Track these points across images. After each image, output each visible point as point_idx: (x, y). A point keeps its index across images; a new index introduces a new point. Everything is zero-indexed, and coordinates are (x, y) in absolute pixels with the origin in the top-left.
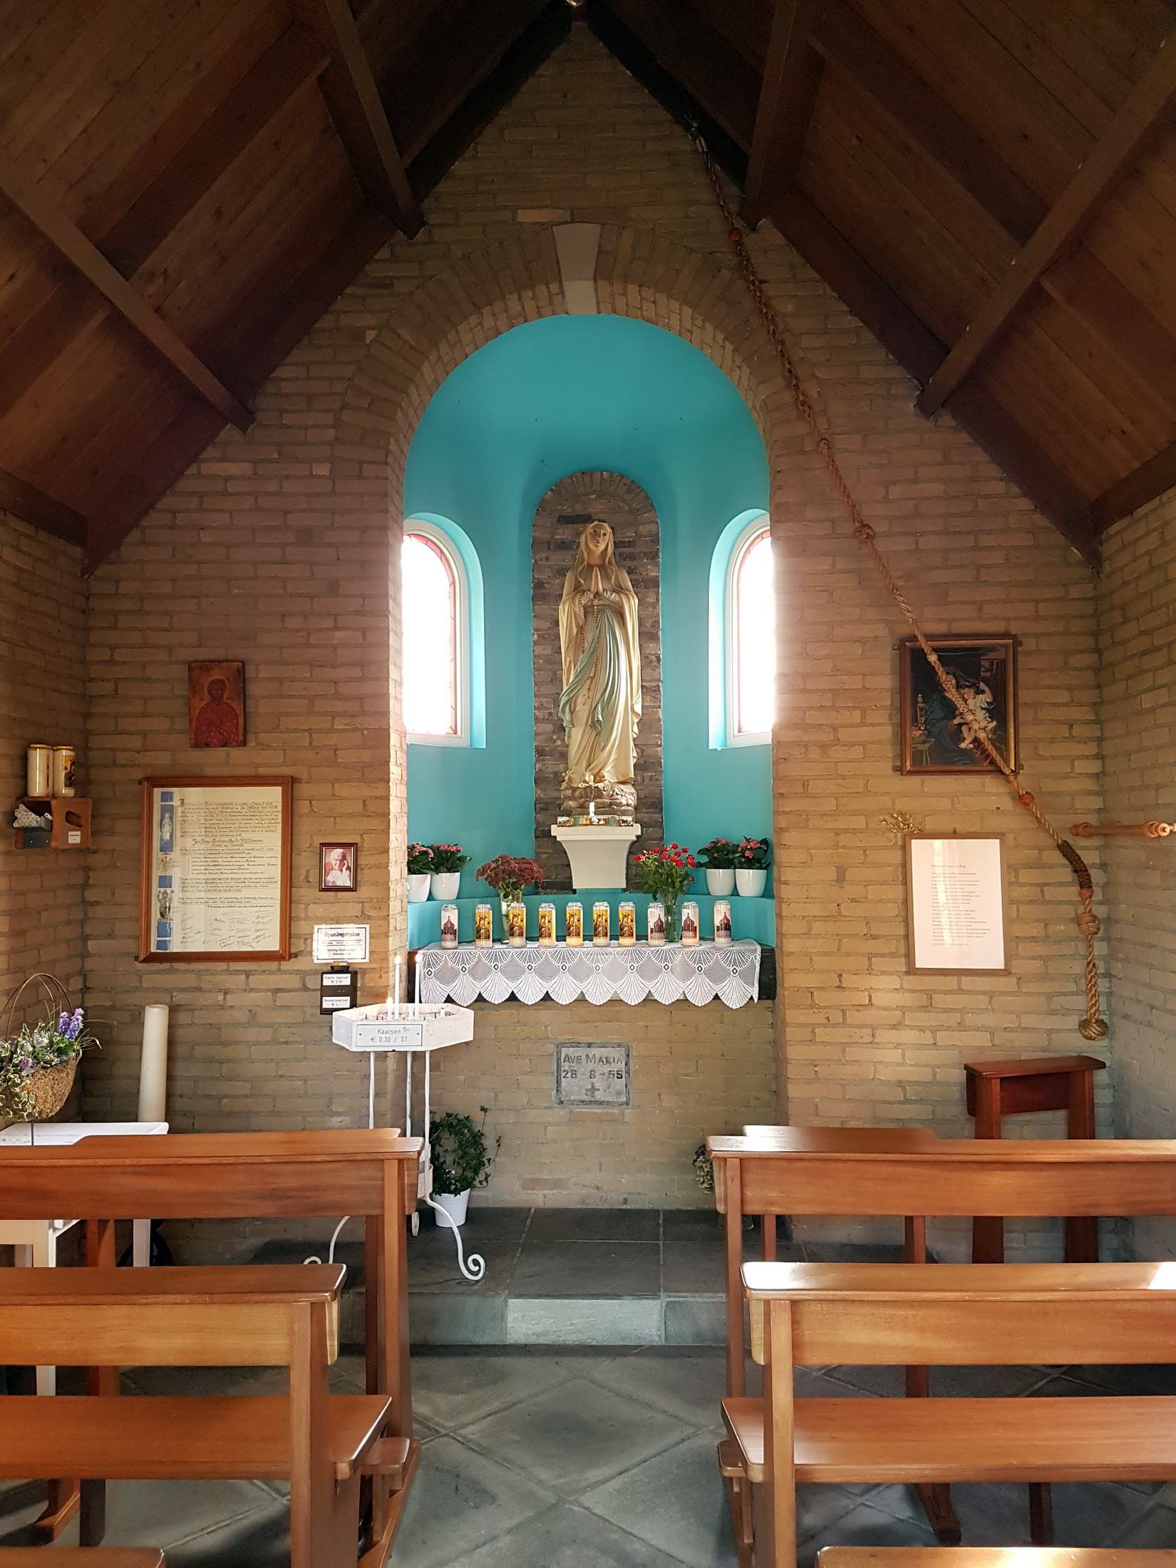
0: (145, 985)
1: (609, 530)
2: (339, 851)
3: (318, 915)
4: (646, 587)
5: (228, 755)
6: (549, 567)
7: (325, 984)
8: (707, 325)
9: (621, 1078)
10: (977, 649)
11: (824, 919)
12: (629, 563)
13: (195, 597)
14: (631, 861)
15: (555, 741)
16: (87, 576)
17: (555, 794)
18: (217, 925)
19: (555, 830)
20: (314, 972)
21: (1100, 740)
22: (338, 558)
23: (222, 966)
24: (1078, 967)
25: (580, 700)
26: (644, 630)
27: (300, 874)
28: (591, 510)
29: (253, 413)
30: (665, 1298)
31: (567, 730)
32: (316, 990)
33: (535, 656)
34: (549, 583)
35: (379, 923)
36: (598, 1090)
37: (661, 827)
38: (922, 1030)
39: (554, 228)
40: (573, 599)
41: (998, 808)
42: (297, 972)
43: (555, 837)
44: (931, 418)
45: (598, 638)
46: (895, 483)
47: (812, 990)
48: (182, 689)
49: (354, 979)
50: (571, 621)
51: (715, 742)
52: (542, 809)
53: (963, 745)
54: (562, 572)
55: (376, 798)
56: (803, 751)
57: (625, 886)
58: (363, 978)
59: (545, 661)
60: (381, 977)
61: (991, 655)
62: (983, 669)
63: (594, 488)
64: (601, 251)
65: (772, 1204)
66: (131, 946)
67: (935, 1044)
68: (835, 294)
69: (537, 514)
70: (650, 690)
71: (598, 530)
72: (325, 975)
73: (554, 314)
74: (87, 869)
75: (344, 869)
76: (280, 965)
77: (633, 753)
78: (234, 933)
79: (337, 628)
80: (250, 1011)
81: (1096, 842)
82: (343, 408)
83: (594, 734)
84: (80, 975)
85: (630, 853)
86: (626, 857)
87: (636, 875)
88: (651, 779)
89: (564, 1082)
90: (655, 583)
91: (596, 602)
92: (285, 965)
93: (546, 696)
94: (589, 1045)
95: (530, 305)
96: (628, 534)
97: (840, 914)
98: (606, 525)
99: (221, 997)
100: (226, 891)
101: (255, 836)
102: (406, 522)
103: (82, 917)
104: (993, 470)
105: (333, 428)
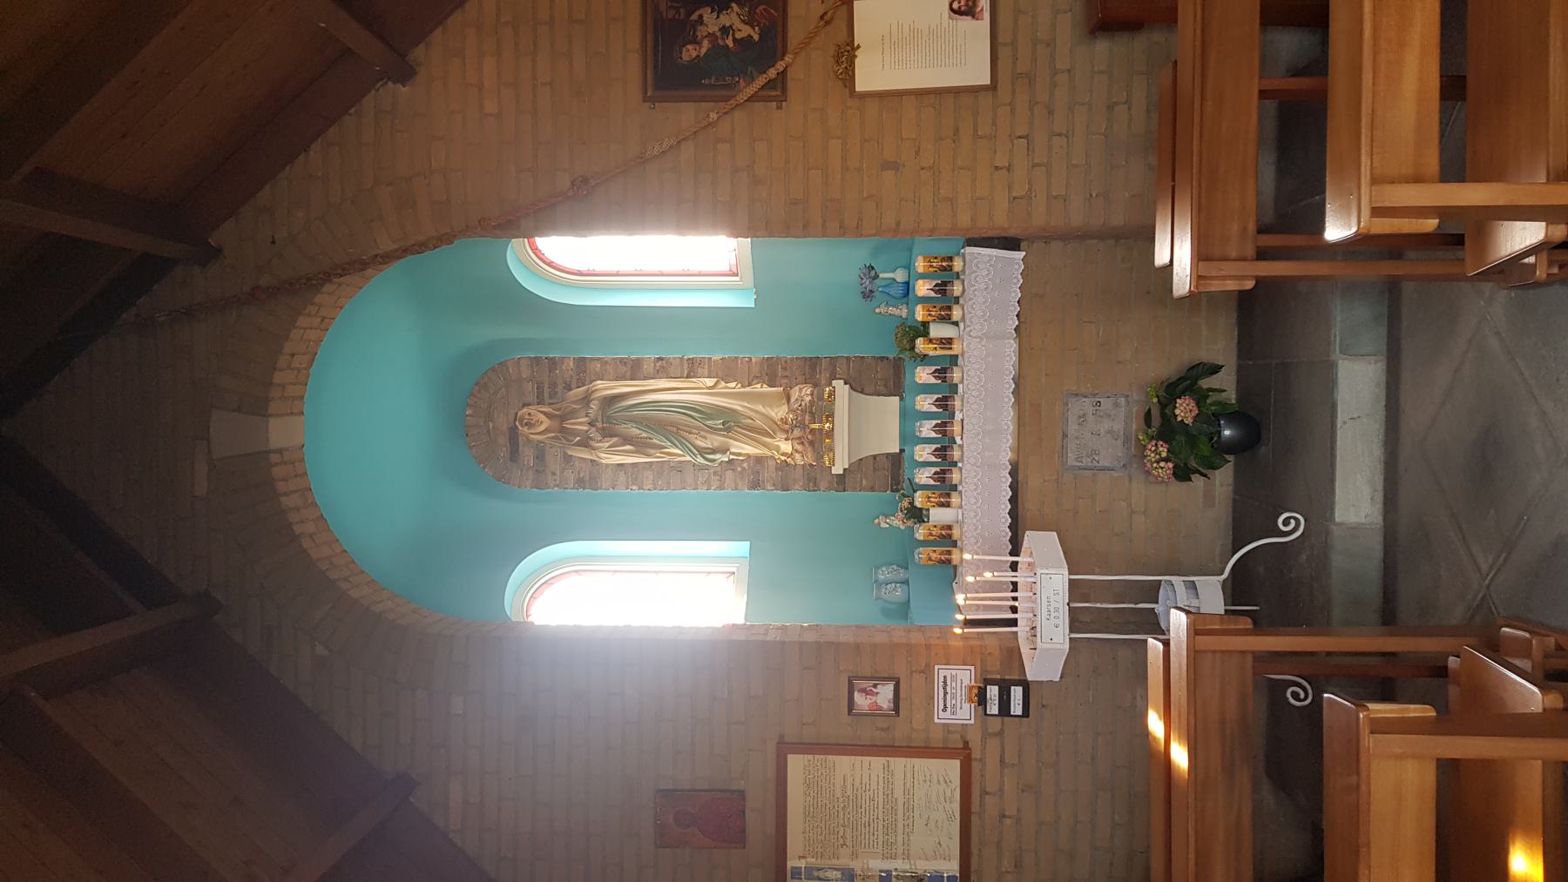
1: (525, 410)
4: (585, 372)
6: (562, 471)
7: (997, 713)
9: (1099, 402)
12: (560, 389)
14: (871, 392)
15: (744, 469)
17: (799, 471)
18: (932, 825)
19: (838, 470)
23: (975, 819)
26: (628, 374)
30: (1336, 355)
31: (731, 457)
32: (1003, 723)
33: (655, 489)
36: (1112, 427)
43: (845, 470)
45: (636, 423)
47: (1012, 198)
51: (747, 301)
52: (815, 484)
53: (756, 37)
54: (568, 459)
57: (898, 398)
60: (990, 654)
64: (239, 410)
65: (1245, 229)
67: (1069, 71)
68: (288, 168)
70: (691, 369)
71: (525, 421)
72: (988, 713)
73: (302, 460)
77: (758, 388)
80: (1023, 791)
83: (735, 428)
85: (862, 392)
88: (784, 369)
89: (1104, 463)
90: (581, 361)
91: (599, 425)
92: (976, 754)
94: (1065, 436)
98: (520, 413)
99: (1008, 821)
101: (839, 783)
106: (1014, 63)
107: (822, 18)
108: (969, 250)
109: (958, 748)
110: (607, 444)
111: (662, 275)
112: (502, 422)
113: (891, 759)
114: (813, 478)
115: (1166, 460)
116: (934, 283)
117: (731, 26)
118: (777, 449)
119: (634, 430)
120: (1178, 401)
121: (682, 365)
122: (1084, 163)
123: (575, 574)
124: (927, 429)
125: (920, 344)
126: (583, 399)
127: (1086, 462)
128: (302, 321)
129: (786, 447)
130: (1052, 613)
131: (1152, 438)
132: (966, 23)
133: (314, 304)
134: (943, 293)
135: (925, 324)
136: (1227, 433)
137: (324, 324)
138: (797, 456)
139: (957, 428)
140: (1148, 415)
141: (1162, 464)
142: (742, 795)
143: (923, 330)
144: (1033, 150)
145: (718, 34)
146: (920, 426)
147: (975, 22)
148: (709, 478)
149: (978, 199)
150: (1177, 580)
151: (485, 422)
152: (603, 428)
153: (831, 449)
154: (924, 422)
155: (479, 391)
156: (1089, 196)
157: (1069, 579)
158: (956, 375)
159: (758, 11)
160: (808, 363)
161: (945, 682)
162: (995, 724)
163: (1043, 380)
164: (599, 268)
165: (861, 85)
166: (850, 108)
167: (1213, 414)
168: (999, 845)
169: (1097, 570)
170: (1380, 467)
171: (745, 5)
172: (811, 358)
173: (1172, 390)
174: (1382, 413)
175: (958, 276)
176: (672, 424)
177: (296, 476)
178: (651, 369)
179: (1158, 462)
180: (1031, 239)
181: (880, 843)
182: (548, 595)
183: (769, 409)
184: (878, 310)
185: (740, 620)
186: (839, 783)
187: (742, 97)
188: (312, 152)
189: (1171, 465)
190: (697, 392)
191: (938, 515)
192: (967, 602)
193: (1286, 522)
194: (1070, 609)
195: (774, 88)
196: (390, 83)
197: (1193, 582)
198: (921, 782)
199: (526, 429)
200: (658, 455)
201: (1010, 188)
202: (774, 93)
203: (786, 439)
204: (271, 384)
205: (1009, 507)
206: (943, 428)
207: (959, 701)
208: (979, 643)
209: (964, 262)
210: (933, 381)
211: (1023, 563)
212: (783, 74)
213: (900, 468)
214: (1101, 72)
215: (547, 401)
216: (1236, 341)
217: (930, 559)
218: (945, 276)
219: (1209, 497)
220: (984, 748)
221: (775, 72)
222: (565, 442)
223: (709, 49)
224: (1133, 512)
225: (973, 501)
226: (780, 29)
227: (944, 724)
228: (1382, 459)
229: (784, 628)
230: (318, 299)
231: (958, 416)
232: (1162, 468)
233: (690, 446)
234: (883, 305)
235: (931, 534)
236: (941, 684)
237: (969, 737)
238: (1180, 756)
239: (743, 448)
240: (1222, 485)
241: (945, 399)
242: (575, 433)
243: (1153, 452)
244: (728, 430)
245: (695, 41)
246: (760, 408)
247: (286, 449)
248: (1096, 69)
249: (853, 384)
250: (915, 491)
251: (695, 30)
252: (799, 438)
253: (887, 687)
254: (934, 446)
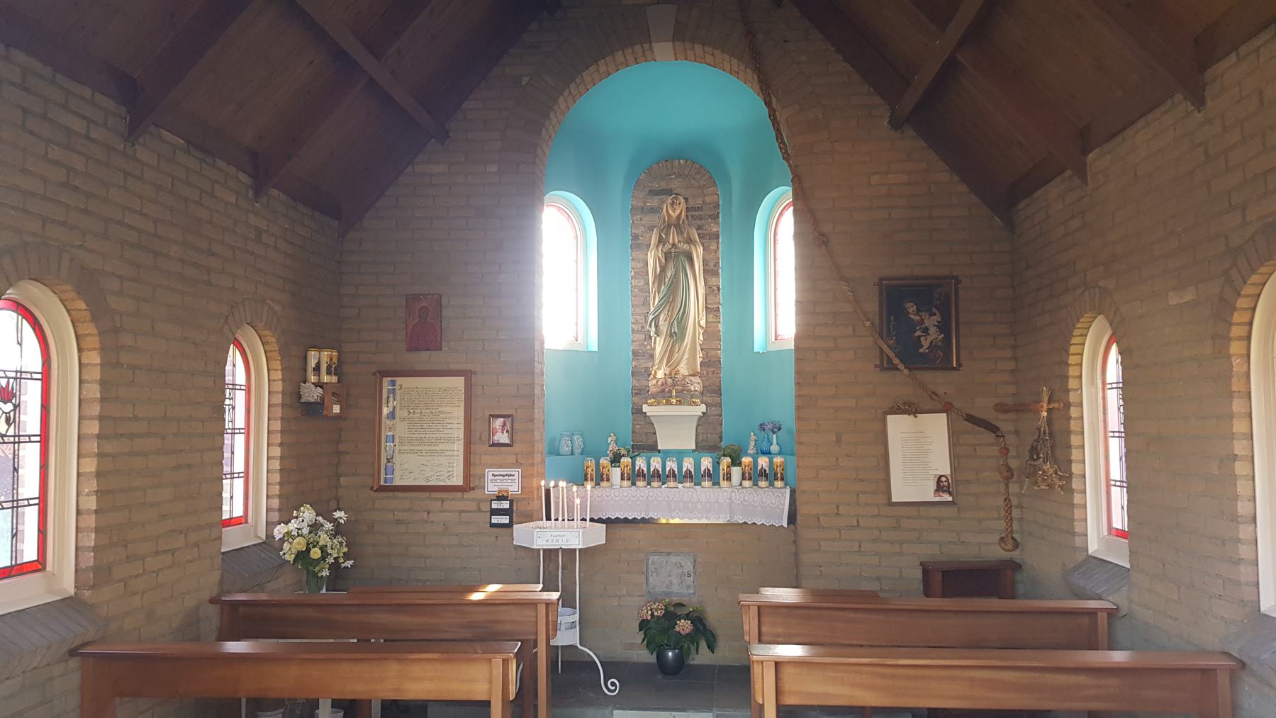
1: (683, 200)
2: (501, 420)
5: (430, 356)
6: (643, 225)
7: (493, 507)
12: (698, 222)
14: (699, 431)
15: (646, 346)
17: (645, 383)
19: (645, 408)
21: (1014, 347)
23: (427, 495)
24: (1000, 502)
25: (662, 317)
26: (707, 268)
31: (653, 338)
34: (642, 236)
37: (721, 406)
38: (892, 543)
40: (657, 246)
41: (945, 393)
42: (474, 500)
45: (675, 275)
46: (876, 173)
49: (511, 504)
50: (656, 266)
51: (758, 347)
53: (921, 350)
54: (651, 229)
57: (694, 448)
58: (517, 503)
59: (640, 291)
68: (833, 49)
69: (634, 189)
70: (712, 310)
73: (646, 61)
75: (505, 432)
76: (463, 494)
77: (700, 355)
78: (433, 473)
80: (444, 525)
81: (1012, 416)
83: (672, 340)
85: (698, 425)
86: (695, 428)
87: (703, 440)
89: (651, 579)
91: (673, 250)
92: (467, 495)
94: (669, 554)
96: (698, 203)
98: (681, 197)
99: (425, 515)
100: (428, 445)
101: (446, 409)
107: (934, 393)
108: (788, 491)
109: (470, 484)
110: (660, 255)
111: (775, 289)
112: (675, 184)
114: (640, 392)
115: (652, 615)
118: (659, 368)
120: (689, 622)
123: (575, 235)
124: (671, 465)
126: (690, 239)
127: (652, 568)
129: (660, 374)
130: (555, 538)
132: (932, 486)
134: (760, 475)
135: (740, 464)
136: (670, 654)
137: (736, 73)
138: (655, 382)
139: (672, 484)
140: (681, 605)
141: (650, 612)
143: (736, 462)
144: (849, 530)
146: (673, 461)
148: (640, 323)
150: (576, 617)
152: (671, 253)
153: (658, 404)
154: (676, 463)
157: (575, 549)
158: (707, 484)
159: (939, 351)
160: (717, 388)
161: (511, 475)
162: (485, 507)
165: (891, 419)
168: (410, 510)
172: (720, 390)
173: (698, 621)
175: (772, 485)
176: (674, 299)
177: (636, 58)
179: (651, 610)
181: (410, 436)
182: (562, 219)
183: (685, 362)
184: (752, 434)
186: (446, 409)
187: (881, 342)
188: (844, 64)
189: (649, 618)
190: (696, 314)
191: (616, 473)
192: (561, 489)
193: (613, 684)
194: (556, 550)
195: (888, 363)
197: (576, 627)
198: (449, 461)
199: (670, 201)
200: (654, 289)
201: (825, 515)
202: (885, 363)
203: (665, 374)
204: (693, 43)
205: (622, 518)
206: (672, 475)
207: (499, 484)
208: (535, 496)
209: (781, 488)
210: (703, 469)
211: (586, 524)
213: (648, 450)
214: (901, 573)
215: (689, 214)
216: (731, 664)
217: (587, 467)
218: (771, 476)
219: (631, 646)
220: (469, 500)
221: (897, 363)
224: (620, 597)
225: (625, 494)
227: (485, 475)
231: (680, 486)
232: (647, 612)
234: (756, 437)
235: (603, 468)
236: (509, 473)
237: (477, 491)
238: (476, 596)
239: (659, 346)
241: (691, 477)
242: (667, 234)
244: (671, 336)
245: (918, 312)
246: (686, 356)
247: (652, 52)
249: (703, 418)
252: (666, 383)
253: (507, 439)
254: (660, 470)
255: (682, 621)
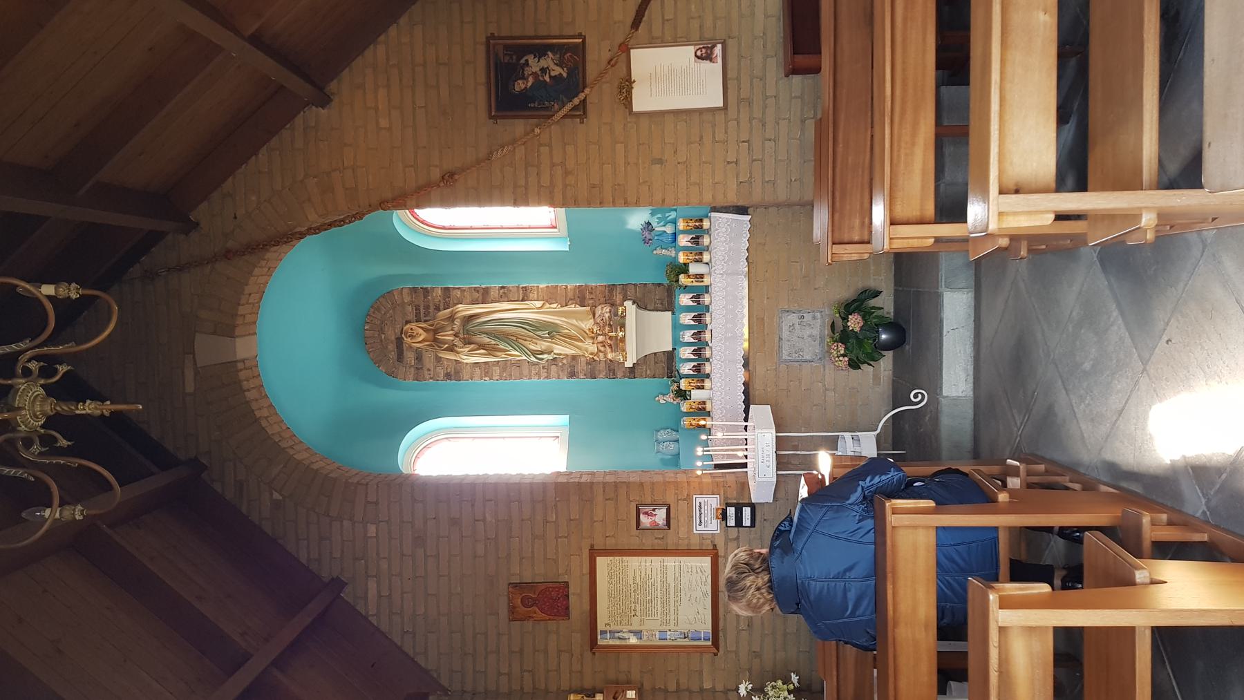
0: (734, 649)
1: (408, 326)
2: (642, 516)
3: (686, 530)
4: (449, 297)
8: (266, 257)
10: (496, 64)
11: (689, 176)
13: (463, 618)
14: (652, 308)
15: (564, 364)
16: (450, 693)
17: (603, 365)
18: (693, 600)
19: (629, 364)
20: (726, 533)
22: (434, 518)
25: (532, 347)
27: (658, 544)
28: (393, 338)
29: (333, 579)
30: (942, 289)
31: (555, 356)
32: (738, 531)
34: (447, 369)
35: (692, 487)
38: (765, 107)
39: (198, 366)
40: (458, 353)
41: (610, 50)
42: (726, 544)
44: (332, 97)
45: (487, 334)
47: (739, 183)
48: (529, 625)
49: (731, 505)
51: (564, 246)
52: (614, 374)
53: (565, 75)
54: (439, 359)
55: (604, 491)
56: (569, 188)
57: (670, 313)
61: (501, 55)
62: (511, 61)
63: (377, 335)
64: (214, 333)
65: (864, 222)
66: (707, 658)
67: (775, 97)
68: (243, 166)
72: (728, 525)
74: (654, 689)
77: (573, 308)
79: (484, 520)
82: (328, 516)
83: (558, 336)
84: (727, 693)
87: (662, 304)
89: (807, 357)
92: (721, 553)
93: (530, 371)
94: (780, 339)
95: (252, 384)
97: (685, 162)
98: (405, 328)
101: (631, 574)
102: (405, 472)
103: (687, 693)
104: (369, 53)
105: (342, 521)
106: (739, 91)
108: (714, 215)
110: (467, 349)
111: (502, 228)
113: (666, 558)
115: (844, 356)
116: (691, 236)
117: (547, 68)
119: (487, 339)
120: (850, 316)
121: (518, 291)
122: (786, 158)
124: (688, 336)
125: (682, 278)
126: (450, 317)
128: (257, 271)
131: (836, 341)
132: (706, 64)
133: (265, 260)
135: (686, 265)
137: (270, 272)
140: (833, 326)
141: (841, 358)
142: (566, 585)
143: (684, 269)
145: (539, 73)
147: (712, 64)
149: (717, 183)
150: (847, 435)
151: (379, 335)
154: (685, 332)
155: (374, 313)
156: (789, 180)
157: (776, 436)
158: (706, 299)
159: (566, 57)
160: (607, 289)
161: (700, 506)
162: (734, 533)
163: (765, 302)
164: (458, 224)
165: (637, 108)
166: (630, 122)
167: (875, 325)
169: (803, 429)
170: (971, 360)
171: (557, 53)
172: (609, 286)
173: (849, 308)
174: (972, 325)
178: (497, 296)
180: (756, 207)
181: (659, 613)
182: (428, 454)
183: (580, 322)
185: (563, 469)
188: (260, 155)
189: (846, 359)
192: (705, 453)
193: (916, 396)
196: (314, 108)
199: (409, 339)
204: (236, 315)
206: (698, 335)
207: (709, 518)
208: (722, 480)
209: (711, 222)
210: (691, 303)
212: (584, 101)
215: (423, 318)
217: (691, 425)
219: (876, 378)
221: (578, 101)
222: (437, 348)
223: (533, 83)
226: (581, 69)
228: (972, 355)
229: (593, 474)
230: (268, 255)
232: (841, 361)
233: (526, 350)
235: (691, 408)
236: (698, 507)
239: (561, 349)
240: (885, 370)
243: (835, 350)
244: (552, 337)
245: (523, 78)
246: (574, 322)
248: (793, 95)
250: (681, 379)
251: (523, 70)
255: (849, 324)
